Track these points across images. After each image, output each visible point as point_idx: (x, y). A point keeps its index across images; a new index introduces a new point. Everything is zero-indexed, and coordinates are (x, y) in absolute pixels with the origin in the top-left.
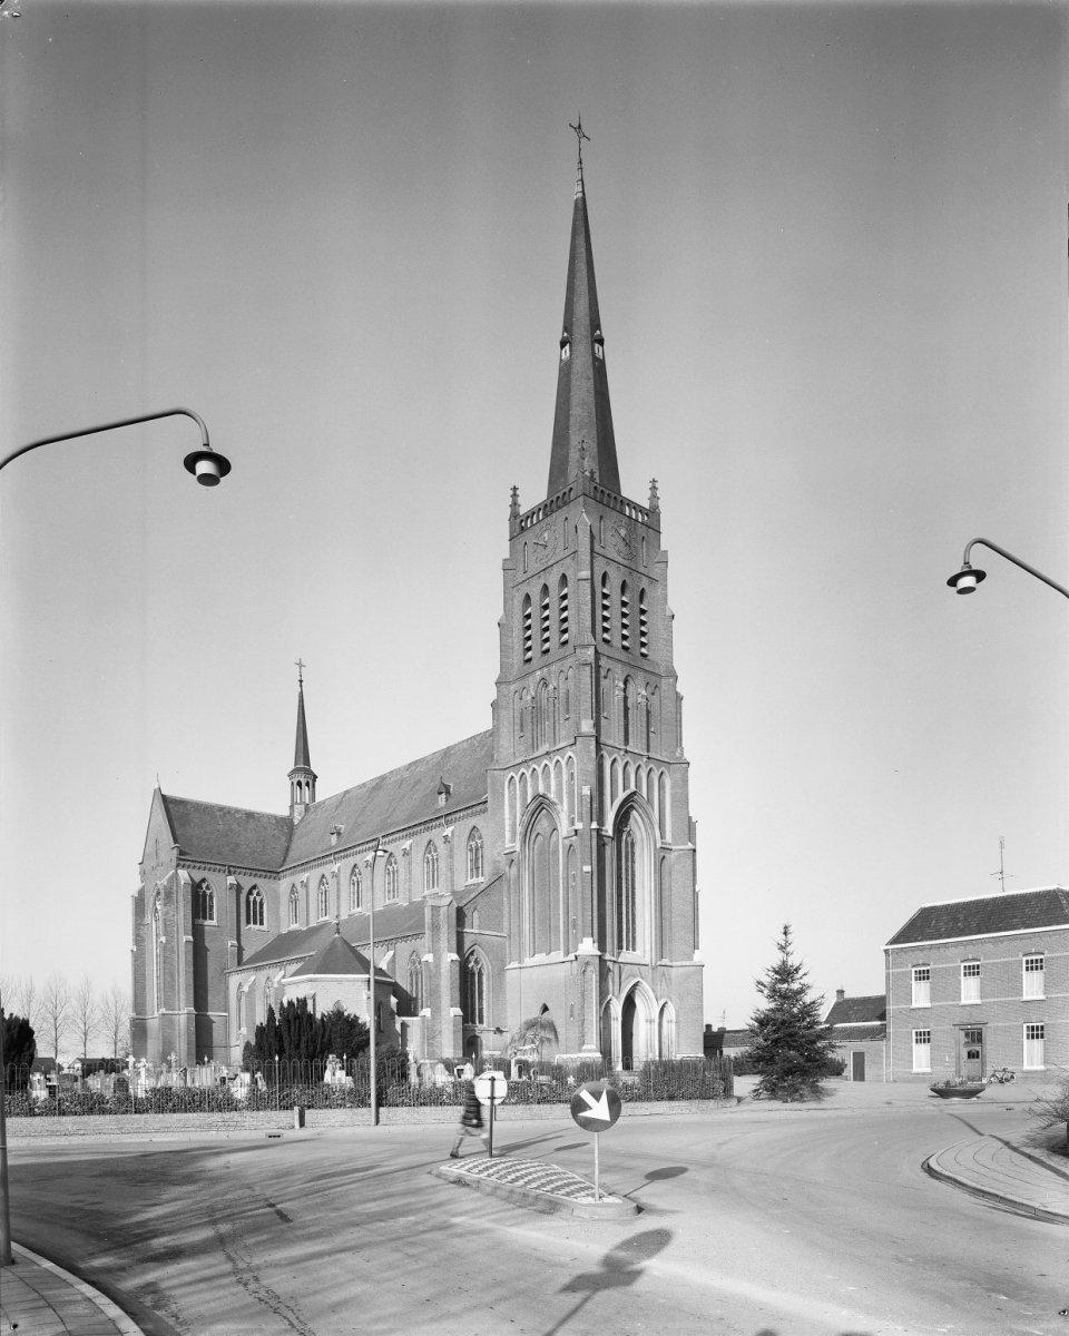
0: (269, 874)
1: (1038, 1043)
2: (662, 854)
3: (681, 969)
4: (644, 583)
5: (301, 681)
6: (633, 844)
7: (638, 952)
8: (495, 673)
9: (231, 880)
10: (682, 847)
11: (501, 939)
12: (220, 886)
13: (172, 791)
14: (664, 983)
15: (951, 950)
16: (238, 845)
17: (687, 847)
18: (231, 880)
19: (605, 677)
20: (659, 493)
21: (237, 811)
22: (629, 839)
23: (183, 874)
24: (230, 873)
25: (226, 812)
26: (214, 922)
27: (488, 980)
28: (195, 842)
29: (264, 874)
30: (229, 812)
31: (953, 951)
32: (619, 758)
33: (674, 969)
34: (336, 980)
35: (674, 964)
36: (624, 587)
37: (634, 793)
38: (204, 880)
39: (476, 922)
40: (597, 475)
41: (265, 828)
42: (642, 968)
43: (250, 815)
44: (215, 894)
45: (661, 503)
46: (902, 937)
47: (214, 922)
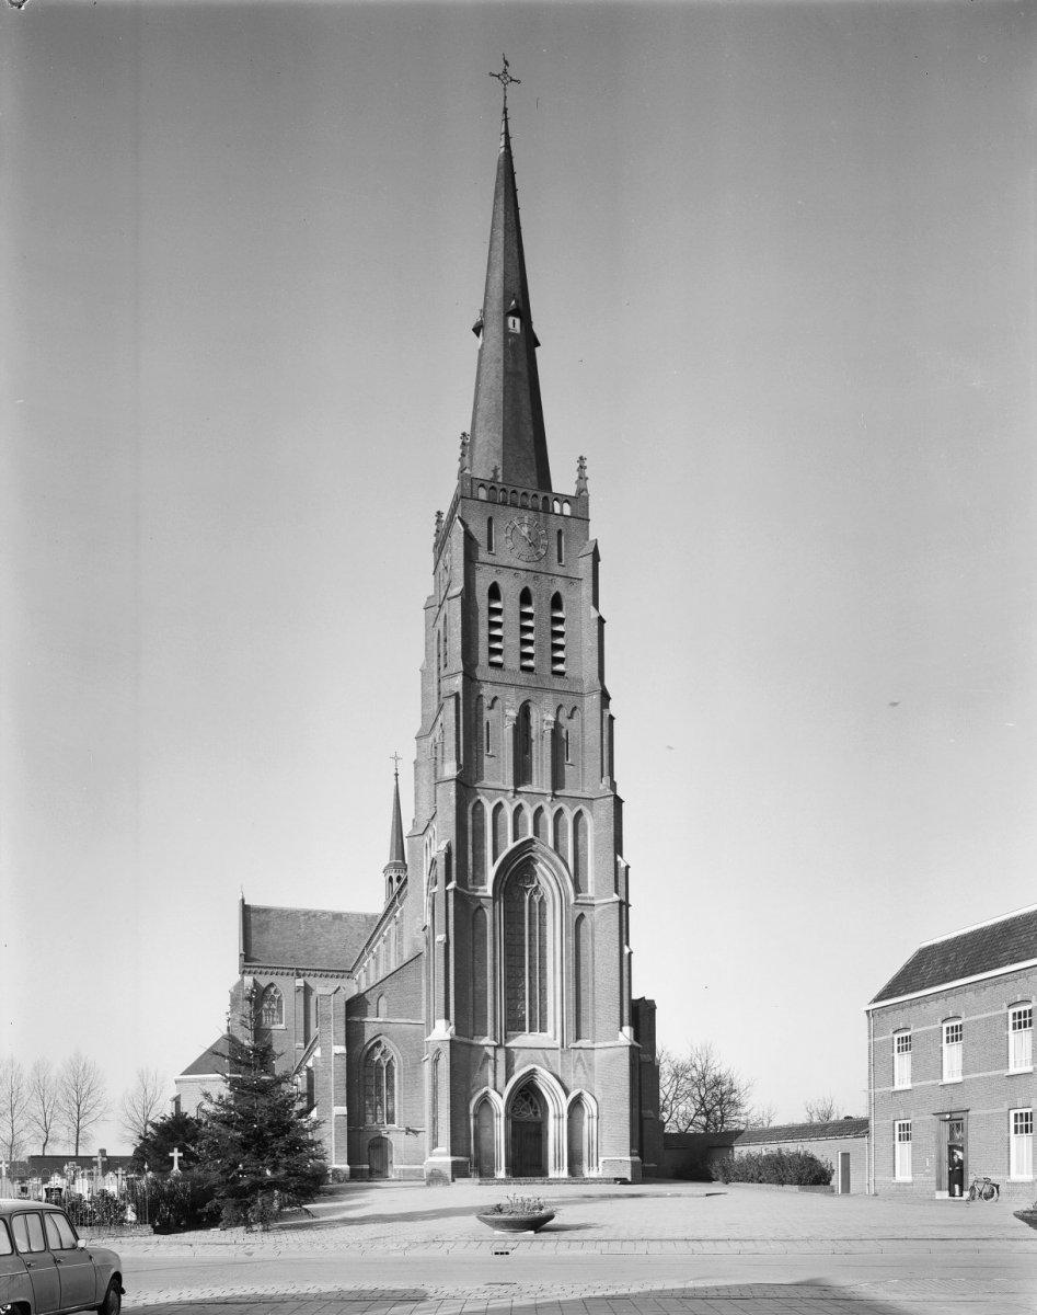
0: (341, 974)
1: (907, 1145)
2: (578, 912)
3: (604, 1052)
4: (559, 586)
5: (397, 775)
6: (542, 902)
7: (550, 1033)
8: (416, 726)
9: (300, 982)
10: (606, 900)
11: (419, 1027)
12: (287, 987)
13: (268, 896)
14: (579, 1067)
15: (934, 1005)
16: (316, 948)
17: (610, 900)
18: (300, 982)
19: (491, 708)
20: (587, 473)
21: (324, 913)
22: (536, 898)
23: (249, 980)
24: (299, 976)
25: (310, 915)
26: (282, 1026)
27: (399, 1074)
28: (270, 947)
29: (336, 974)
30: (315, 916)
31: (934, 1006)
32: (505, 803)
33: (596, 1051)
34: (200, 1081)
35: (595, 1046)
36: (526, 598)
37: (531, 841)
38: (272, 985)
39: (383, 1009)
40: (500, 472)
41: (352, 928)
42: (548, 1053)
43: (337, 917)
44: (283, 999)
45: (590, 485)
46: (890, 991)
47: (282, 1026)
